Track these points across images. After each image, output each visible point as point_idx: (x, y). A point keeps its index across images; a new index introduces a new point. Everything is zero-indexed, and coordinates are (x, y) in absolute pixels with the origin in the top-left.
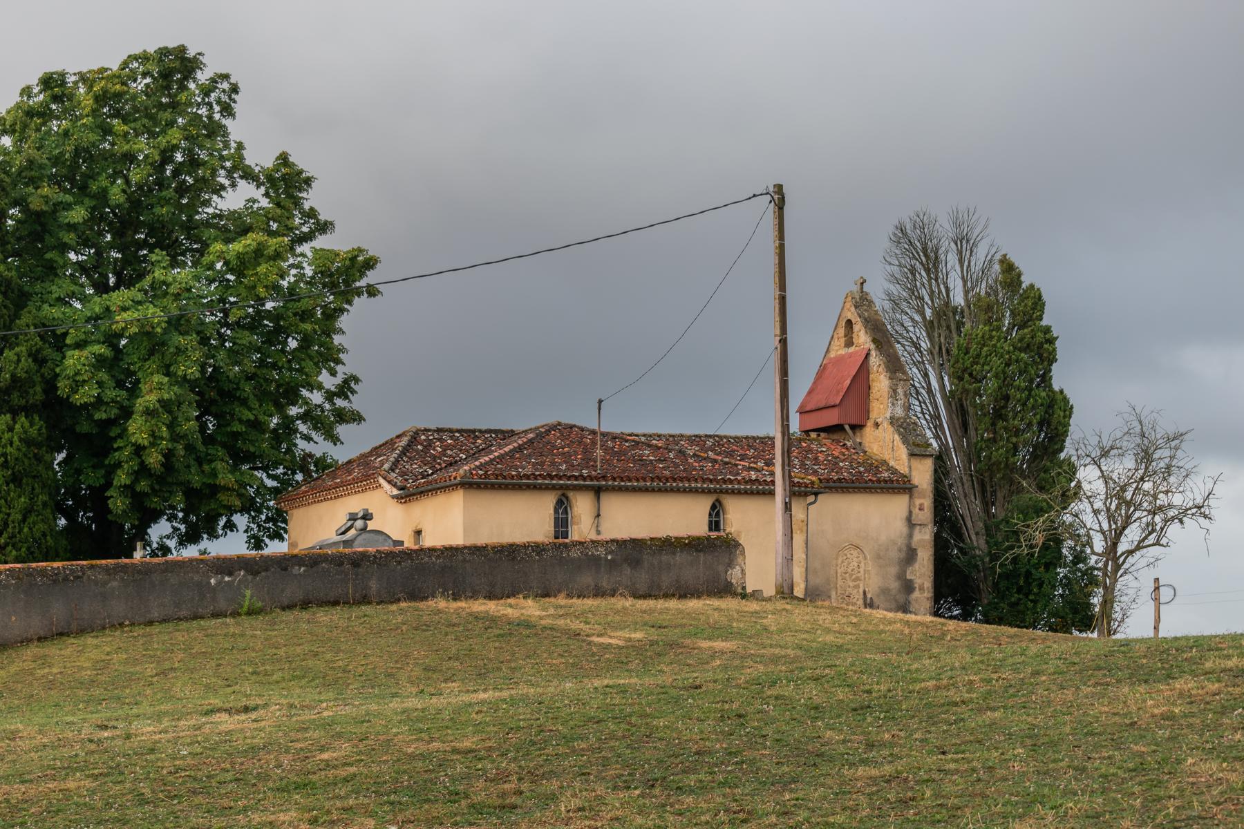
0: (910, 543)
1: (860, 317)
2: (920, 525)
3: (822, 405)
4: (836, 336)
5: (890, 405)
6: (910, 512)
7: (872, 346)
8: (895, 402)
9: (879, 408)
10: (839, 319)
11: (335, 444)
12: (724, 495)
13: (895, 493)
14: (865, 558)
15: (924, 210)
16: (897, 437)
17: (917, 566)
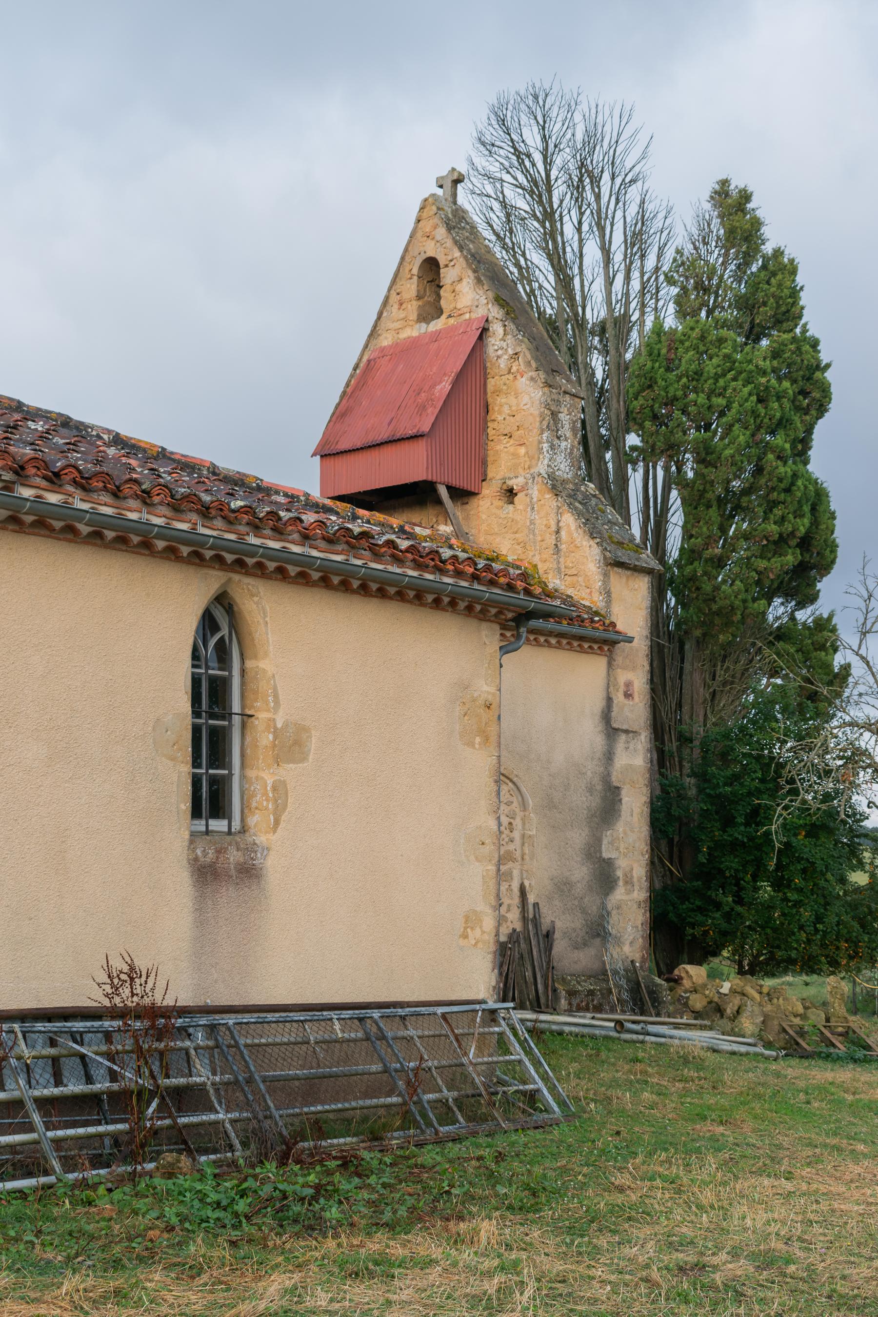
0: (609, 775)
1: (461, 248)
2: (627, 732)
3: (384, 436)
4: (394, 298)
5: (546, 446)
6: (609, 700)
7: (496, 312)
8: (556, 441)
9: (515, 455)
10: (403, 258)
11: (746, 196)
12: (247, 580)
13: (582, 650)
14: (524, 806)
15: (547, 86)
16: (569, 520)
17: (620, 827)
